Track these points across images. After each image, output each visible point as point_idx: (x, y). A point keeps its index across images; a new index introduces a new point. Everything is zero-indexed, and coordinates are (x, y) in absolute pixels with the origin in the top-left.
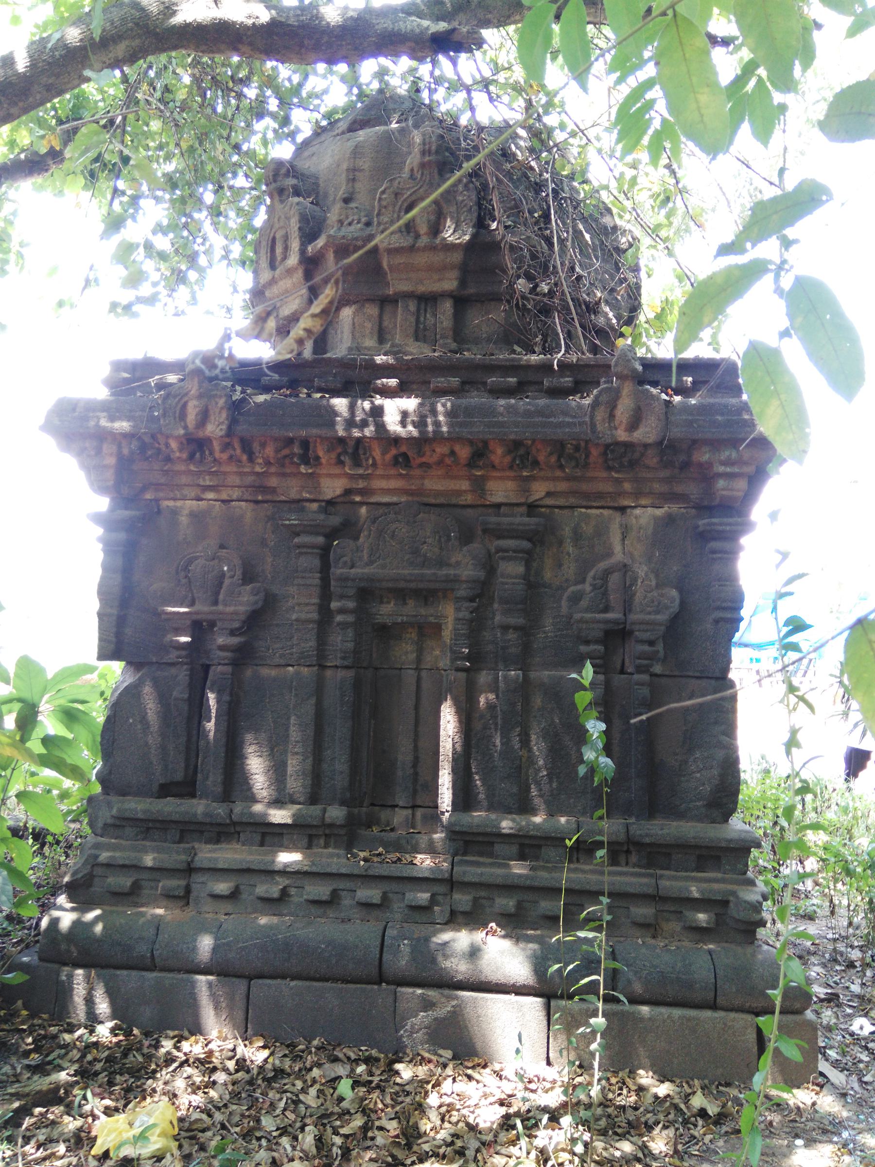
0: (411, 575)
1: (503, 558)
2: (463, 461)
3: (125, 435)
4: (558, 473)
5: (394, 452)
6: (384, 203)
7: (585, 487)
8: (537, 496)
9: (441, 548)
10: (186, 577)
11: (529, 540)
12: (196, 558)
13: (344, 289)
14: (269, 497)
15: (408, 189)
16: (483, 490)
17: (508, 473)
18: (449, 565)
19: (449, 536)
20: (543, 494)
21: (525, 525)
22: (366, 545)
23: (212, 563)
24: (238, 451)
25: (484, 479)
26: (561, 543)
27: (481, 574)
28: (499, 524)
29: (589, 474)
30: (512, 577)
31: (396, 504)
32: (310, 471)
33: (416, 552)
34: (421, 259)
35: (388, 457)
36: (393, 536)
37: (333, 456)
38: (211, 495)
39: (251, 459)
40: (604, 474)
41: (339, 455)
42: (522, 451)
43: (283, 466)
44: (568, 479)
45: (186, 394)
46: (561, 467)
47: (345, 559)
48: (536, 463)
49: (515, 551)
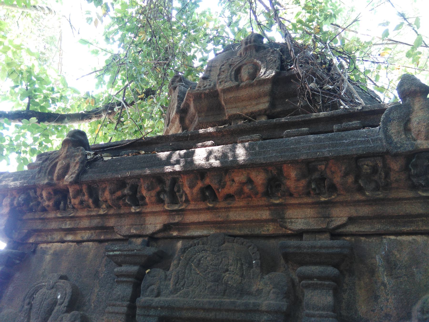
0: (210, 303)
1: (308, 286)
2: (261, 189)
3: (15, 189)
4: (358, 197)
5: (200, 185)
6: (222, 70)
7: (390, 210)
8: (338, 222)
9: (242, 276)
10: (29, 303)
11: (336, 266)
12: (41, 287)
13: (199, 120)
14: (109, 237)
15: (237, 62)
16: (283, 218)
17: (306, 200)
18: (249, 294)
19: (250, 265)
20: (345, 219)
21: (327, 247)
22: (174, 273)
23: (50, 292)
24: (86, 197)
25: (283, 206)
26: (372, 272)
27: (284, 305)
28: (299, 247)
29: (393, 195)
30: (319, 309)
31: (206, 236)
32: (138, 210)
33: (218, 280)
34: (243, 93)
35: (196, 190)
36: (198, 265)
37: (153, 193)
38: (70, 238)
39: (97, 204)
40: (411, 194)
41: (158, 194)
42: (316, 175)
43: (119, 207)
44: (370, 202)
45: (58, 157)
46: (360, 190)
47: (153, 287)
48: (333, 188)
49: (320, 278)
